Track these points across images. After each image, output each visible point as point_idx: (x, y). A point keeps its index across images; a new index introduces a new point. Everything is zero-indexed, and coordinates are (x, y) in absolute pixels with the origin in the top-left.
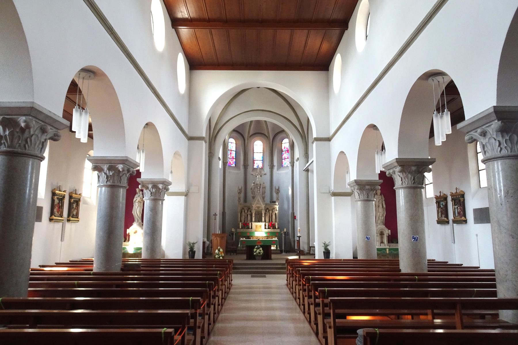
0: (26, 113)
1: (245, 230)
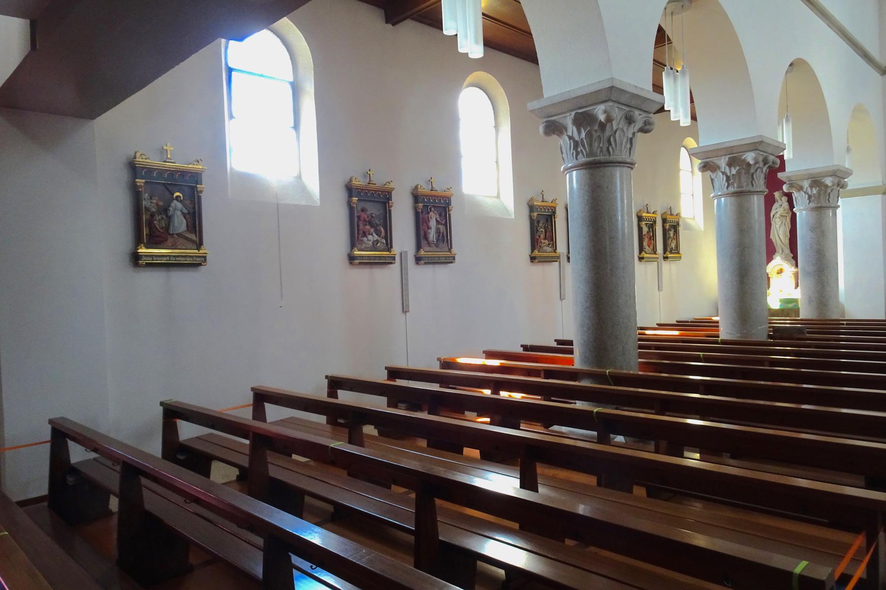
0: (604, 99)
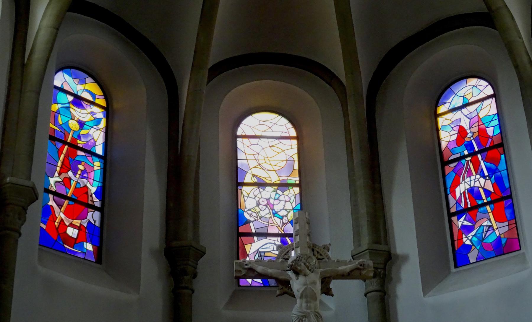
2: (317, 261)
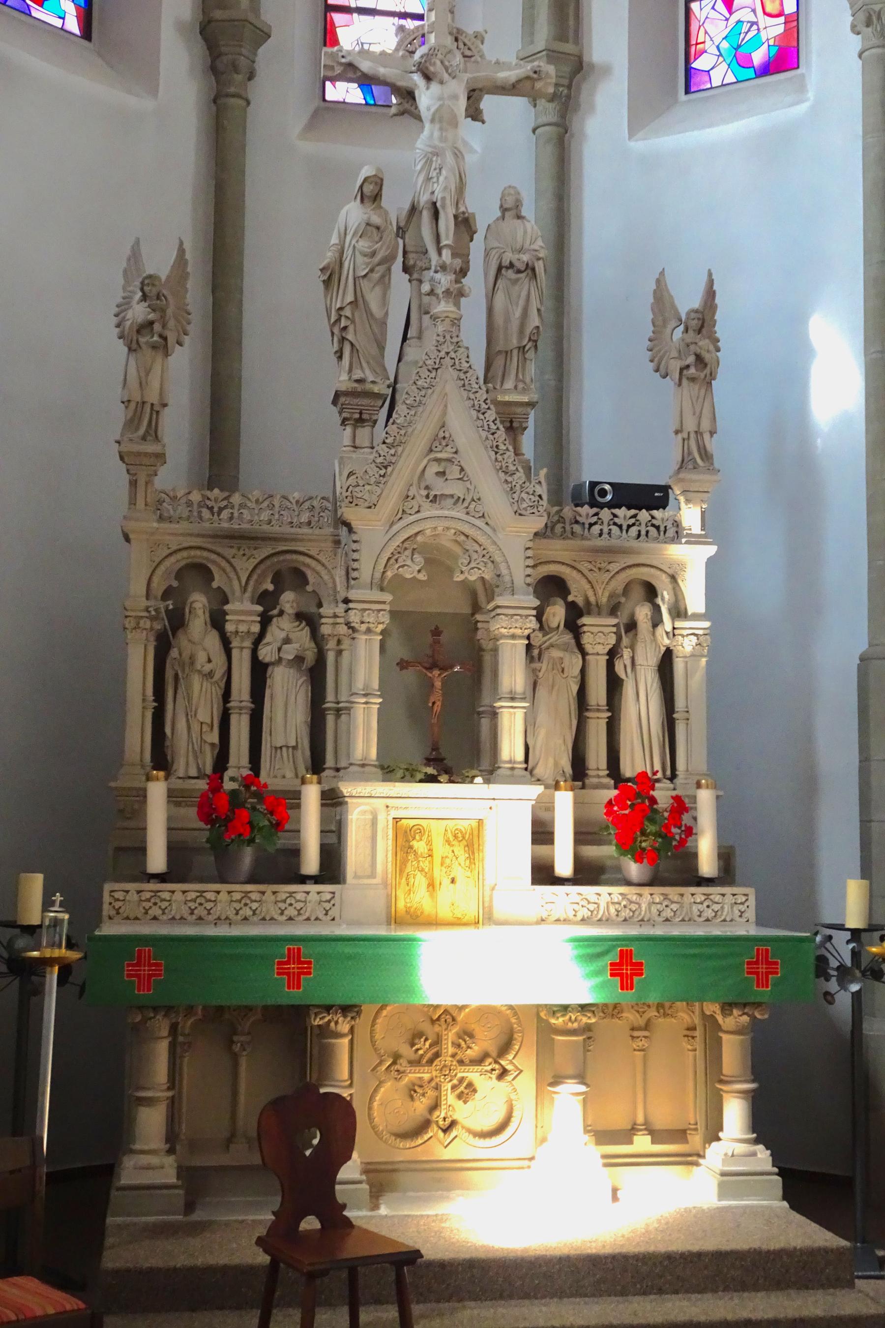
1: (233, 911)
2: (462, 60)
